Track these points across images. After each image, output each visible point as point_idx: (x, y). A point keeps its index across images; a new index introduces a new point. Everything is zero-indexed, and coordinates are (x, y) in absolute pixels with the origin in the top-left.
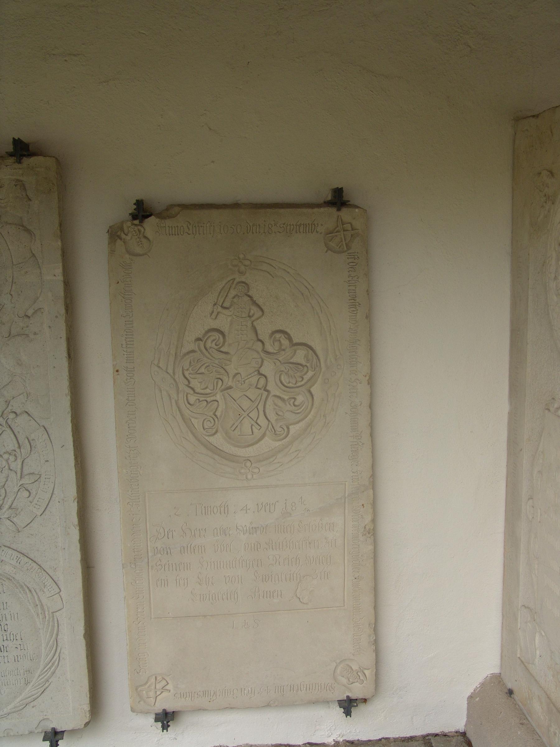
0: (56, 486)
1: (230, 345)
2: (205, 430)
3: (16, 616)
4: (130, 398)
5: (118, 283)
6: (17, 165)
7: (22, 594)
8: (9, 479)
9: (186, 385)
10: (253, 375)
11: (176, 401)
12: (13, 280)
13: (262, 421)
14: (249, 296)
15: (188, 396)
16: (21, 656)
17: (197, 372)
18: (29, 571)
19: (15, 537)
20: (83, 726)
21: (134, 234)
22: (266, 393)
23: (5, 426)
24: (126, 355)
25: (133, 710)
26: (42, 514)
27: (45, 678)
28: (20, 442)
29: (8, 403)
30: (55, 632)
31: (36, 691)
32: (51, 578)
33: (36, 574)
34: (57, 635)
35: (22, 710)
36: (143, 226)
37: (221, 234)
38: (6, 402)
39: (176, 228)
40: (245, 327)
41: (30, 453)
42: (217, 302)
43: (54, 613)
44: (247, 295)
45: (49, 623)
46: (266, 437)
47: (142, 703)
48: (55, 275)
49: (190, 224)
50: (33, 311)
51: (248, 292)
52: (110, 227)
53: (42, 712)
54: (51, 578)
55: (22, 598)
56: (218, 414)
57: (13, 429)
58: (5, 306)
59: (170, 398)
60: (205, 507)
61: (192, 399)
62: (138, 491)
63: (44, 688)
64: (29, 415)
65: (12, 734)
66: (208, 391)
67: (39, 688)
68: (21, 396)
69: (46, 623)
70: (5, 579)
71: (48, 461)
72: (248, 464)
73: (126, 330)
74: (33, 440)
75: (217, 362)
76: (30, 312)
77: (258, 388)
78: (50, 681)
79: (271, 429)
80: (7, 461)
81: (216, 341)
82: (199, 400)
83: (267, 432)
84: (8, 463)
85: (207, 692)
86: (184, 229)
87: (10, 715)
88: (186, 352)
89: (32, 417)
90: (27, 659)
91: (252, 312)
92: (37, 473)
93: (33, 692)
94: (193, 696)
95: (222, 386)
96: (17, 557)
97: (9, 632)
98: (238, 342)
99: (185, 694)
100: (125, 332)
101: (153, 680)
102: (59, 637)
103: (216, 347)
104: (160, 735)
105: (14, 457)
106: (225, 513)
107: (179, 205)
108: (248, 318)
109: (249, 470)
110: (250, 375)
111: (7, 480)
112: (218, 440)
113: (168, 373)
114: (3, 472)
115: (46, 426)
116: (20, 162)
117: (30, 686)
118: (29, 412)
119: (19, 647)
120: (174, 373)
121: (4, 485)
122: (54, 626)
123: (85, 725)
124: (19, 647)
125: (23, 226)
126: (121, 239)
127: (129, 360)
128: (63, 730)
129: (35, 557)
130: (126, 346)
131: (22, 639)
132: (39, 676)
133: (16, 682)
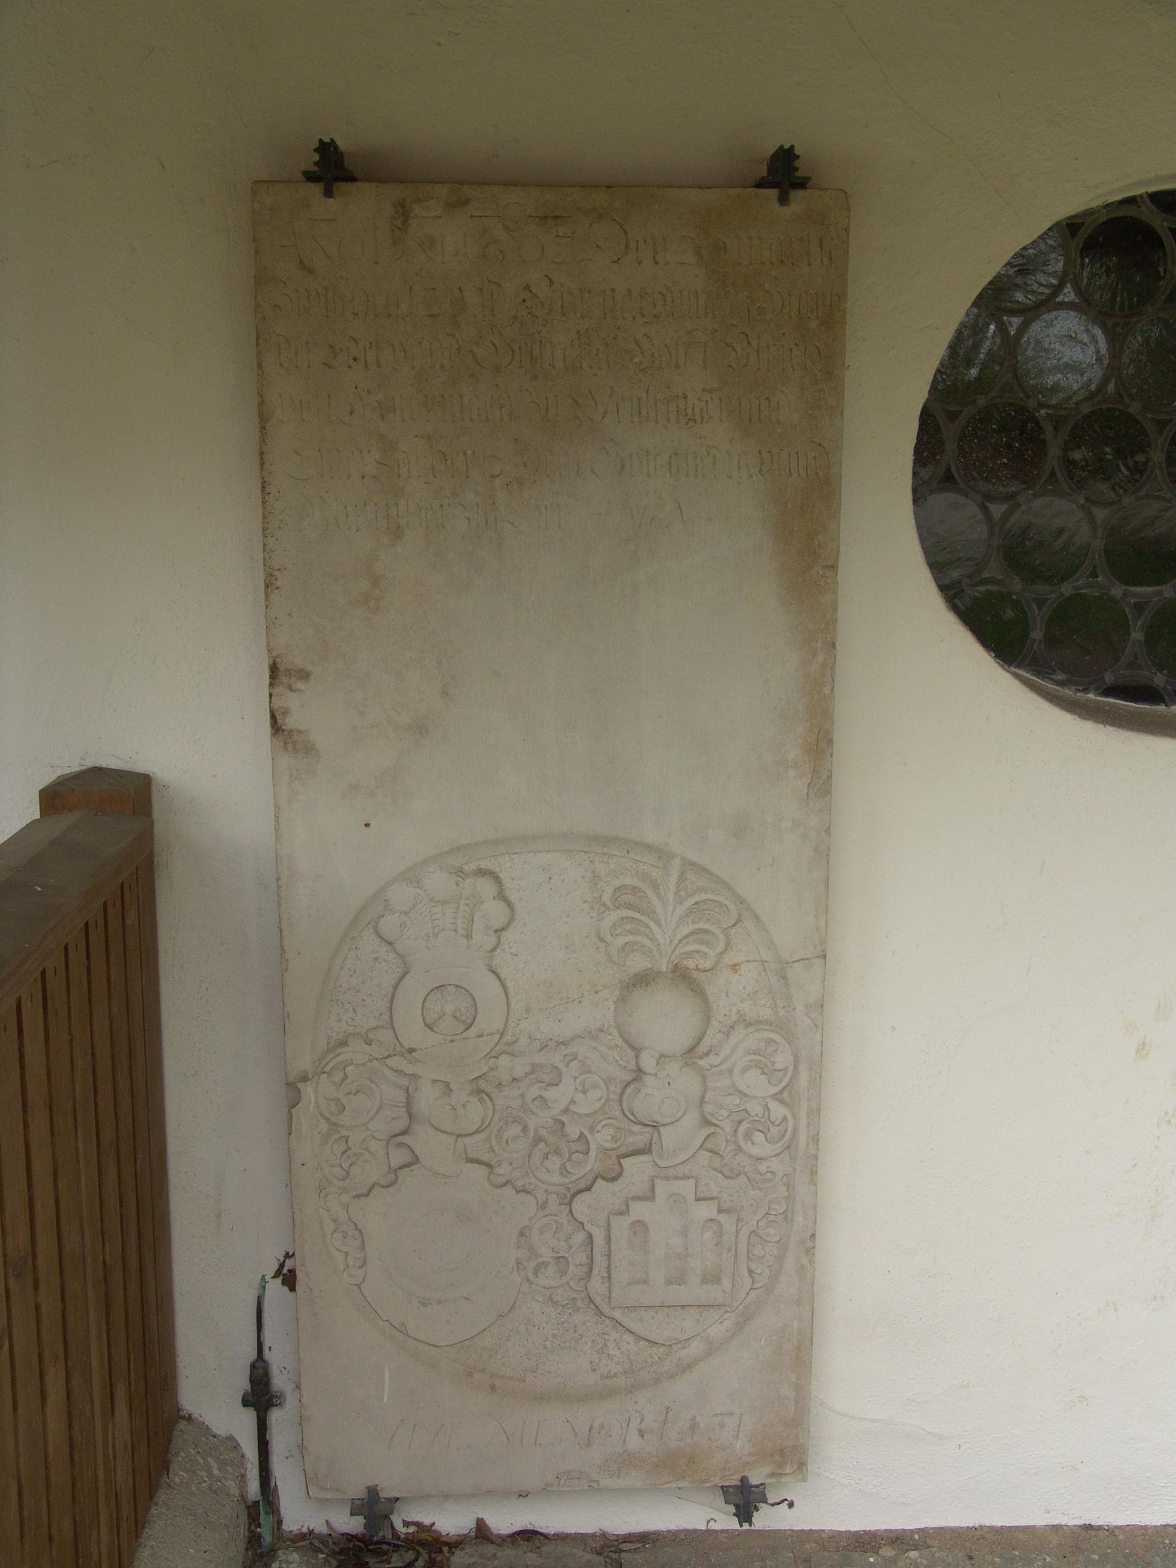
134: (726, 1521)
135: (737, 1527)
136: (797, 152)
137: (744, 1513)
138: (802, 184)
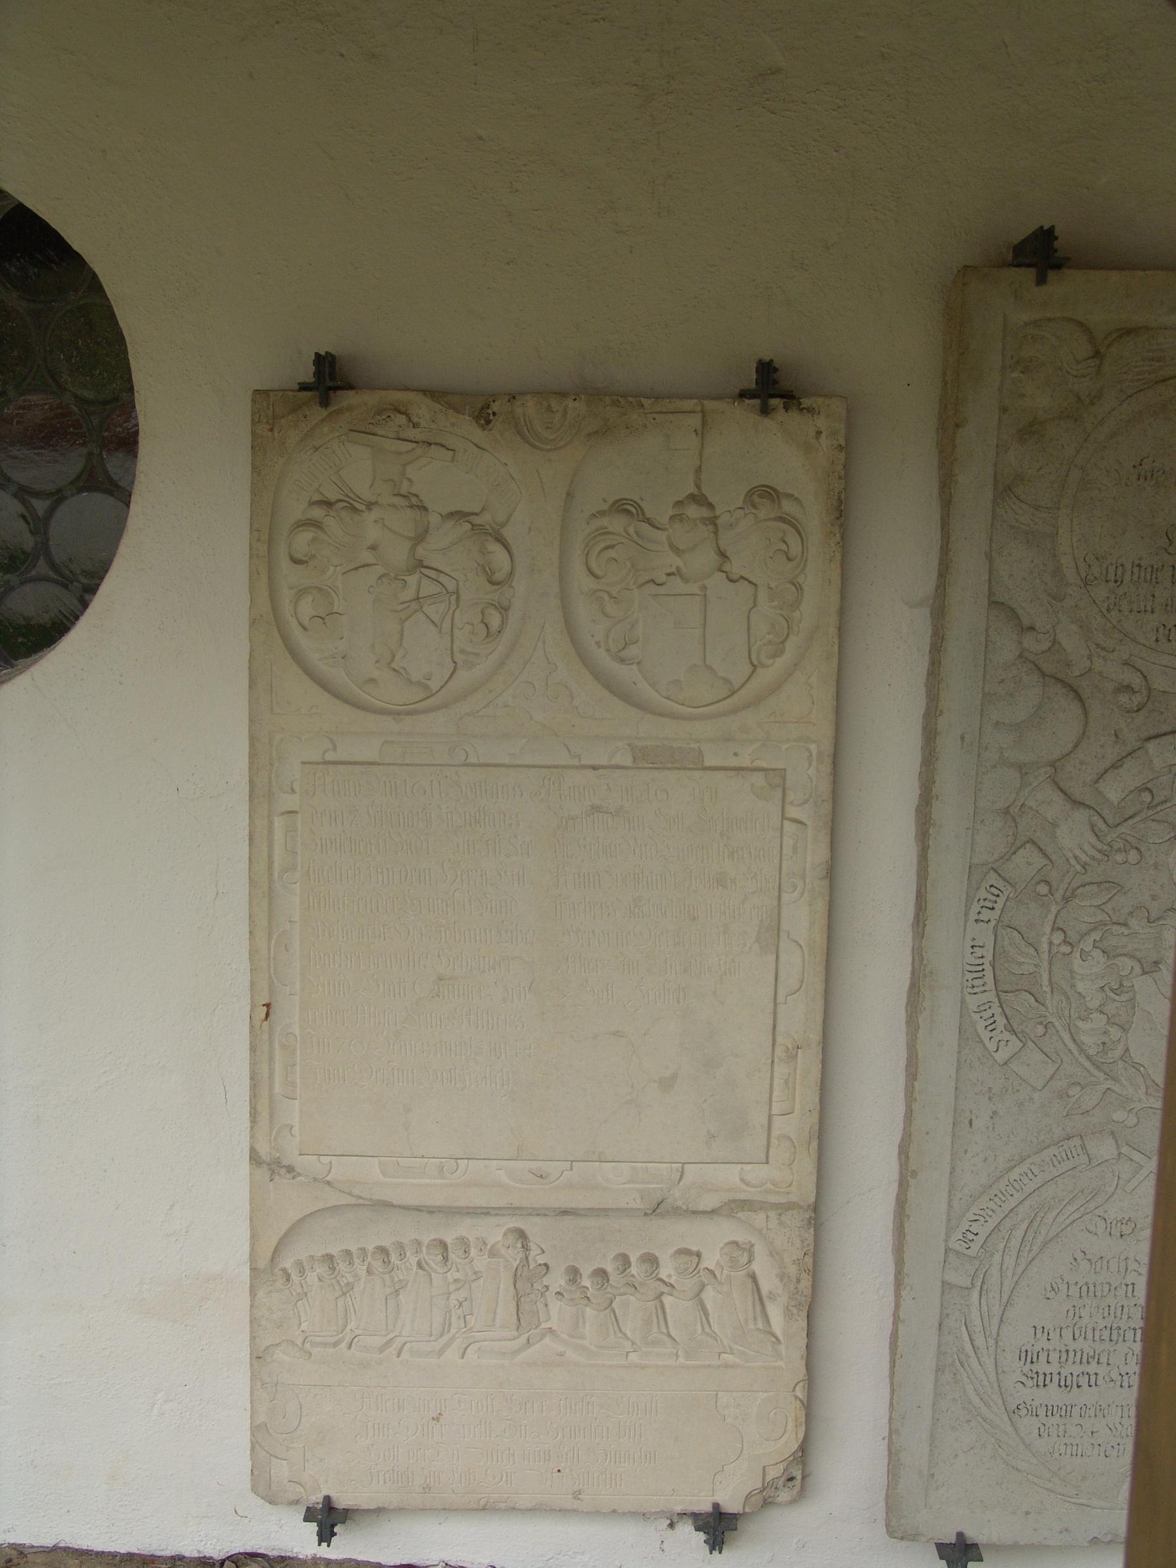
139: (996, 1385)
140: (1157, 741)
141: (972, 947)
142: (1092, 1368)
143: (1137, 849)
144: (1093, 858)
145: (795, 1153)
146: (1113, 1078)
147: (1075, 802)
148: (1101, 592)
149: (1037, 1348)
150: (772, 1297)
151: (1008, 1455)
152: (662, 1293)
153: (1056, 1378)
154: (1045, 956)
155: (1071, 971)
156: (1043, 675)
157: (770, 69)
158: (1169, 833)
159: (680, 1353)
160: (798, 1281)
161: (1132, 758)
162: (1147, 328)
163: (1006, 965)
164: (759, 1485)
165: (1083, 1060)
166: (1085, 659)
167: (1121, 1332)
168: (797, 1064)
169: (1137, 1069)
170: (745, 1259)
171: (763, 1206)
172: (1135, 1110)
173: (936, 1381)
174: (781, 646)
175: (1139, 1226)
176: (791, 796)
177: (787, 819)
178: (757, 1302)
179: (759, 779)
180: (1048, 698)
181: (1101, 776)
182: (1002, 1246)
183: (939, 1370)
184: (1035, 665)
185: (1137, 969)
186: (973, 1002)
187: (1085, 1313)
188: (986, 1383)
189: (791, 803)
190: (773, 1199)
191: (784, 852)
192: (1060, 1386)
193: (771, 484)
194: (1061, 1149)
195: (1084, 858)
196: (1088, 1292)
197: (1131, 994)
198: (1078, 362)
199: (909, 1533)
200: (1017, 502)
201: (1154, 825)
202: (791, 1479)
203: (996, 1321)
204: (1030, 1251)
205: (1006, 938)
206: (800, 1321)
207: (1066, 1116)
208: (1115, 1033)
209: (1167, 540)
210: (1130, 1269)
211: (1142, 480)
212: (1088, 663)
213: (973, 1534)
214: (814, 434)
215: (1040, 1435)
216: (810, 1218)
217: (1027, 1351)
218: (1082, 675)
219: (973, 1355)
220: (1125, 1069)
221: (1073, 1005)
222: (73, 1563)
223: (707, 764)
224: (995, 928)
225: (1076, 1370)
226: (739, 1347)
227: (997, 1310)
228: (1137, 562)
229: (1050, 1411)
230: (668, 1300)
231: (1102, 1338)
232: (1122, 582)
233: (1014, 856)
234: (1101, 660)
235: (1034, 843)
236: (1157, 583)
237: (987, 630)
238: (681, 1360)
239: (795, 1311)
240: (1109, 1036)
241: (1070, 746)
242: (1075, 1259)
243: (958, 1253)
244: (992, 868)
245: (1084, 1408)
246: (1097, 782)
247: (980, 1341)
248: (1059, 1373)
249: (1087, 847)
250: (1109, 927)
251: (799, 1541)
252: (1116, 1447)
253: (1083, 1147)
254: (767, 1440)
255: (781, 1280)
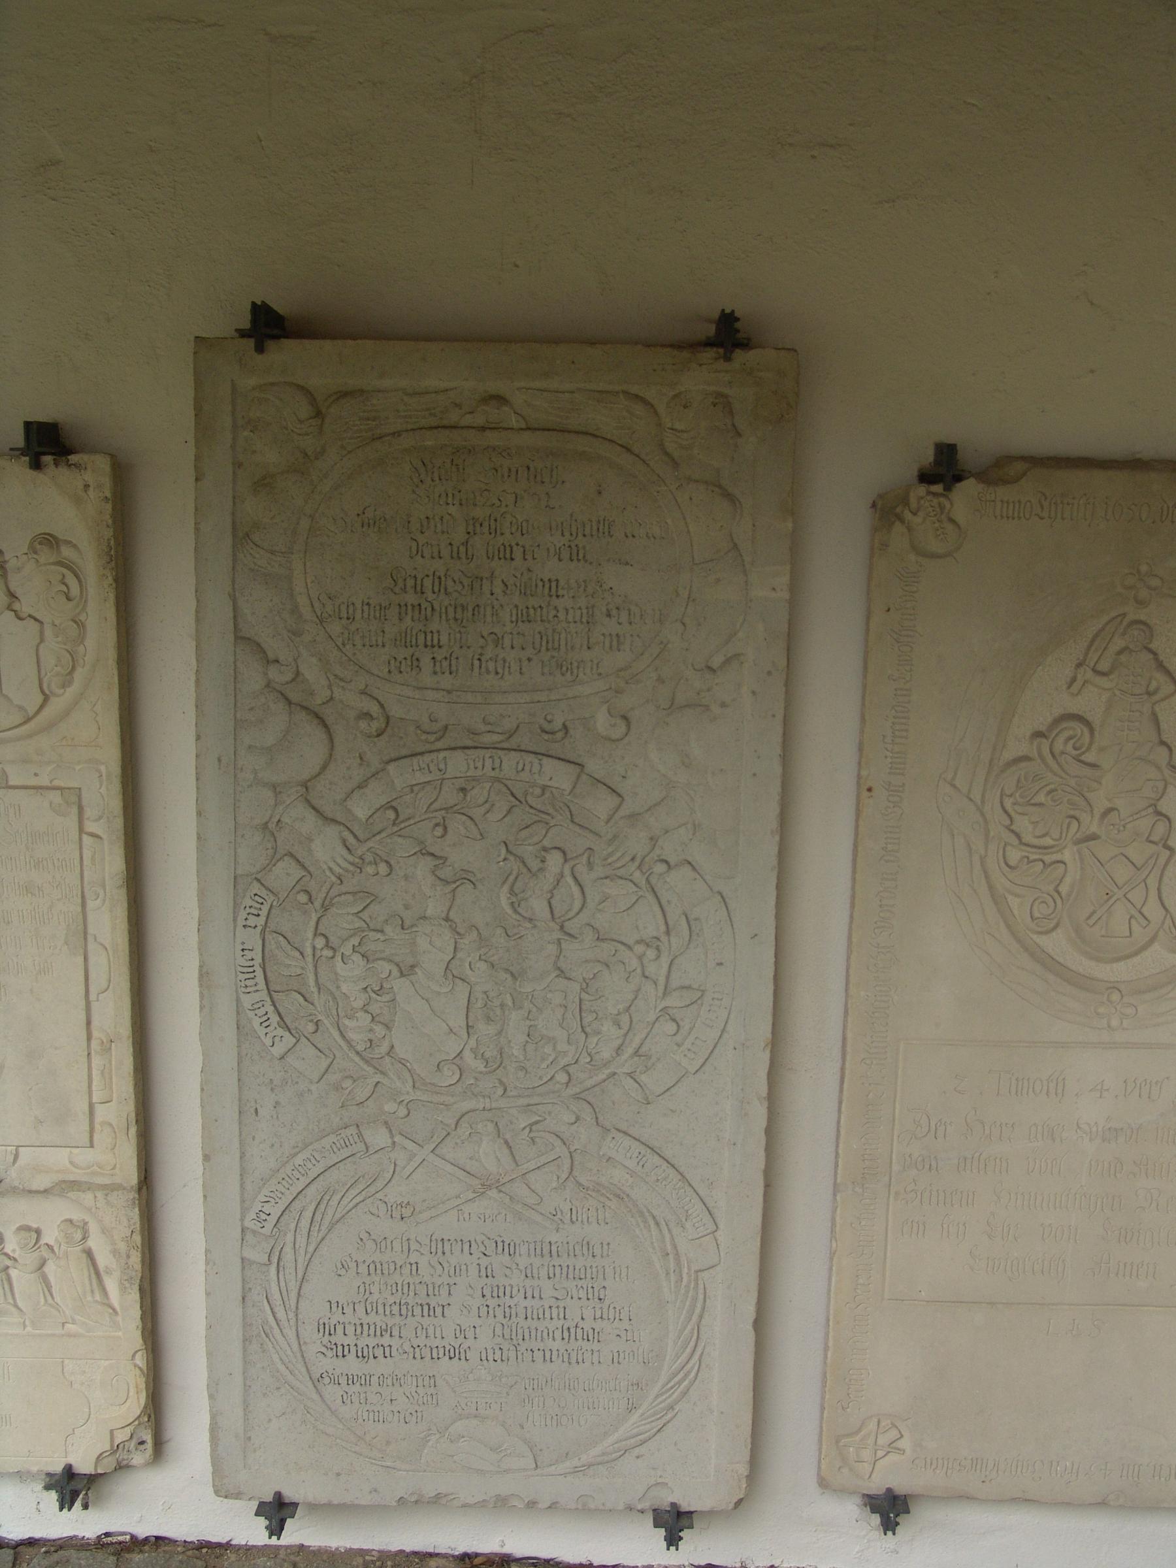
0: (732, 1016)
1: (1102, 749)
2: (1035, 922)
3: (624, 1271)
4: (890, 847)
5: (889, 610)
6: (721, 365)
7: (641, 1230)
8: (640, 996)
9: (1004, 826)
10: (1144, 813)
11: (981, 858)
12: (689, 594)
13: (1153, 910)
14: (1150, 651)
15: (1006, 849)
16: (627, 1354)
17: (1029, 800)
18: (659, 1183)
19: (638, 1113)
20: (731, 1506)
21: (930, 512)
22: (1168, 852)
23: (645, 889)
24: (891, 757)
25: (823, 1484)
26: (697, 1071)
27: (669, 1401)
28: (671, 923)
29: (653, 840)
30: (698, 1311)
31: (648, 1426)
32: (702, 1200)
33: (674, 1191)
34: (701, 1317)
35: (616, 1462)
36: (949, 499)
37: (1108, 520)
38: (651, 839)
39: (1017, 505)
40: (1138, 714)
41: (689, 944)
42: (1085, 660)
43: (699, 1273)
44: (1146, 648)
45: (687, 1292)
46: (1156, 944)
47: (845, 1471)
48: (774, 589)
49: (1046, 498)
50: (723, 658)
51: (1151, 642)
52: (880, 496)
53: (653, 1469)
54: (702, 1200)
55: (641, 1236)
56: (1064, 889)
57: (658, 894)
58: (670, 646)
59: (970, 850)
60: (1017, 1080)
61: (1014, 855)
62: (887, 1036)
63: (663, 1421)
64: (694, 869)
65: (592, 1506)
66: (1048, 841)
67: (652, 1422)
68: (682, 831)
69: (683, 1291)
70: (611, 1197)
71: (721, 964)
72: (1115, 997)
73: (896, 708)
74: (696, 919)
75: (1073, 782)
76: (716, 662)
77: (1151, 842)
78: (677, 1408)
79: (1169, 928)
80: (640, 958)
81: (1075, 740)
82: (1028, 858)
83: (1161, 933)
84: (642, 964)
85: (979, 1461)
86: (1032, 507)
87: (592, 1468)
88: (1011, 758)
89: (698, 873)
90: (635, 1361)
91: (1154, 684)
92: (695, 986)
93: (641, 1428)
94: (950, 1466)
95: (1076, 833)
96: (640, 1153)
97: (607, 1302)
98: (1119, 744)
99: (935, 1462)
100: (893, 711)
101: (872, 1425)
102: (703, 1322)
103: (1075, 753)
104: (866, 1541)
105: (656, 952)
106: (1056, 1094)
107: (1023, 458)
108: (1146, 697)
109: (1116, 1009)
110: (1137, 814)
111: (636, 998)
112: (1057, 944)
113: (971, 800)
114: (630, 980)
115: (724, 894)
116: (728, 359)
117: (635, 1417)
118: (693, 863)
119: (623, 1334)
120: (983, 802)
121: (630, 1006)
122: (695, 1299)
123: (735, 1504)
124: (623, 1334)
125: (720, 487)
126: (902, 521)
127: (896, 769)
128: (692, 1510)
129: (674, 1156)
130: (893, 740)
131: (630, 1320)
132: (657, 1397)
133: (611, 1403)
134: (254, 1532)
135: (267, 1541)
136: (737, 314)
137: (276, 1529)
138: (745, 345)
139: (299, 1355)
140: (396, 763)
141: (243, 950)
142: (386, 1340)
143: (387, 862)
144: (347, 871)
145: (116, 1138)
146: (382, 1073)
147: (326, 818)
148: (335, 628)
149: (333, 1322)
150: (108, 1271)
151: (316, 1420)
152: (8, 1267)
153: (353, 1349)
154: (310, 959)
155: (336, 974)
156: (290, 703)
157: (51, 161)
158: (414, 848)
159: (27, 1323)
160: (128, 1257)
161: (376, 779)
162: (362, 391)
163: (275, 967)
164: (107, 1447)
165: (352, 1055)
166: (326, 688)
167: (410, 1307)
168: (111, 1055)
169: (403, 1064)
170: (78, 1235)
171: (89, 1187)
172: (405, 1102)
173: (245, 1350)
174: (68, 677)
175: (417, 1209)
176: (88, 812)
177: (86, 833)
178: (93, 1276)
179: (56, 797)
180: (295, 724)
181: (349, 795)
182: (293, 1226)
183: (246, 1340)
184: (282, 694)
185: (395, 972)
186: (247, 1001)
187: (375, 1289)
188: (289, 1352)
189: (88, 819)
190: (100, 1180)
191: (85, 863)
192: (358, 1357)
193: (51, 532)
194: (339, 1137)
195: (337, 870)
196: (376, 1269)
197: (391, 995)
198: (301, 422)
199: (232, 1492)
200: (254, 547)
201: (400, 840)
202: (142, 1443)
203: (293, 1295)
204: (319, 1230)
205: (273, 942)
206: (133, 1294)
207: (342, 1107)
208: (379, 1030)
209: (393, 582)
210: (412, 1249)
211: (366, 527)
212: (329, 693)
213: (290, 1495)
214: (82, 487)
215: (343, 1402)
216: (134, 1198)
217: (324, 1324)
218: (324, 703)
219: (275, 1326)
220: (392, 1064)
221: (340, 1004)
222: (83, 1559)
223: (11, 783)
224: (263, 931)
225: (372, 1342)
226: (79, 1317)
227: (293, 1286)
228: (366, 601)
229: (351, 1380)
230: (14, 1273)
231: (393, 1313)
232: (354, 618)
233: (274, 868)
234: (340, 690)
235: (291, 855)
236: (386, 620)
237: (235, 662)
238: (29, 1329)
239: (127, 1285)
240: (375, 1033)
241: (317, 769)
242: (361, 1239)
243: (254, 1232)
244: (256, 878)
245: (381, 1377)
246: (345, 800)
247: (281, 1314)
248: (356, 1345)
249: (340, 861)
250: (366, 933)
251: (164, 1502)
252: (414, 1414)
253: (360, 1135)
254: (112, 1405)
255: (114, 1256)
